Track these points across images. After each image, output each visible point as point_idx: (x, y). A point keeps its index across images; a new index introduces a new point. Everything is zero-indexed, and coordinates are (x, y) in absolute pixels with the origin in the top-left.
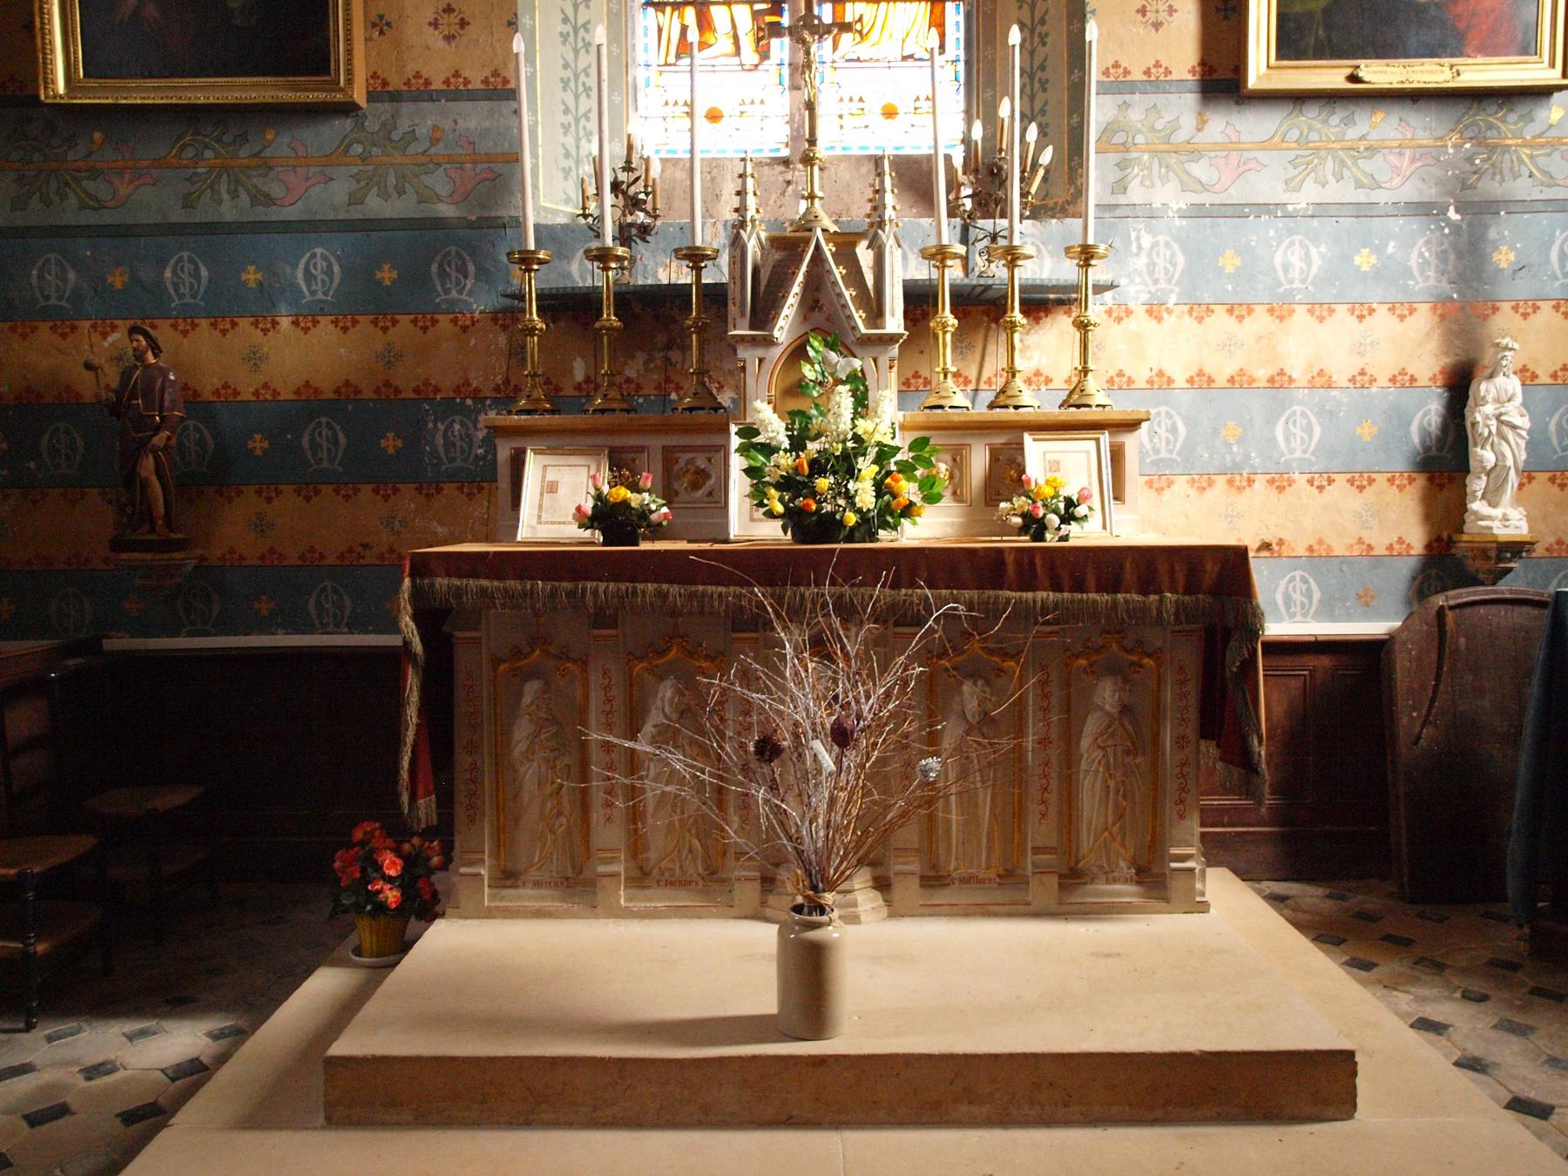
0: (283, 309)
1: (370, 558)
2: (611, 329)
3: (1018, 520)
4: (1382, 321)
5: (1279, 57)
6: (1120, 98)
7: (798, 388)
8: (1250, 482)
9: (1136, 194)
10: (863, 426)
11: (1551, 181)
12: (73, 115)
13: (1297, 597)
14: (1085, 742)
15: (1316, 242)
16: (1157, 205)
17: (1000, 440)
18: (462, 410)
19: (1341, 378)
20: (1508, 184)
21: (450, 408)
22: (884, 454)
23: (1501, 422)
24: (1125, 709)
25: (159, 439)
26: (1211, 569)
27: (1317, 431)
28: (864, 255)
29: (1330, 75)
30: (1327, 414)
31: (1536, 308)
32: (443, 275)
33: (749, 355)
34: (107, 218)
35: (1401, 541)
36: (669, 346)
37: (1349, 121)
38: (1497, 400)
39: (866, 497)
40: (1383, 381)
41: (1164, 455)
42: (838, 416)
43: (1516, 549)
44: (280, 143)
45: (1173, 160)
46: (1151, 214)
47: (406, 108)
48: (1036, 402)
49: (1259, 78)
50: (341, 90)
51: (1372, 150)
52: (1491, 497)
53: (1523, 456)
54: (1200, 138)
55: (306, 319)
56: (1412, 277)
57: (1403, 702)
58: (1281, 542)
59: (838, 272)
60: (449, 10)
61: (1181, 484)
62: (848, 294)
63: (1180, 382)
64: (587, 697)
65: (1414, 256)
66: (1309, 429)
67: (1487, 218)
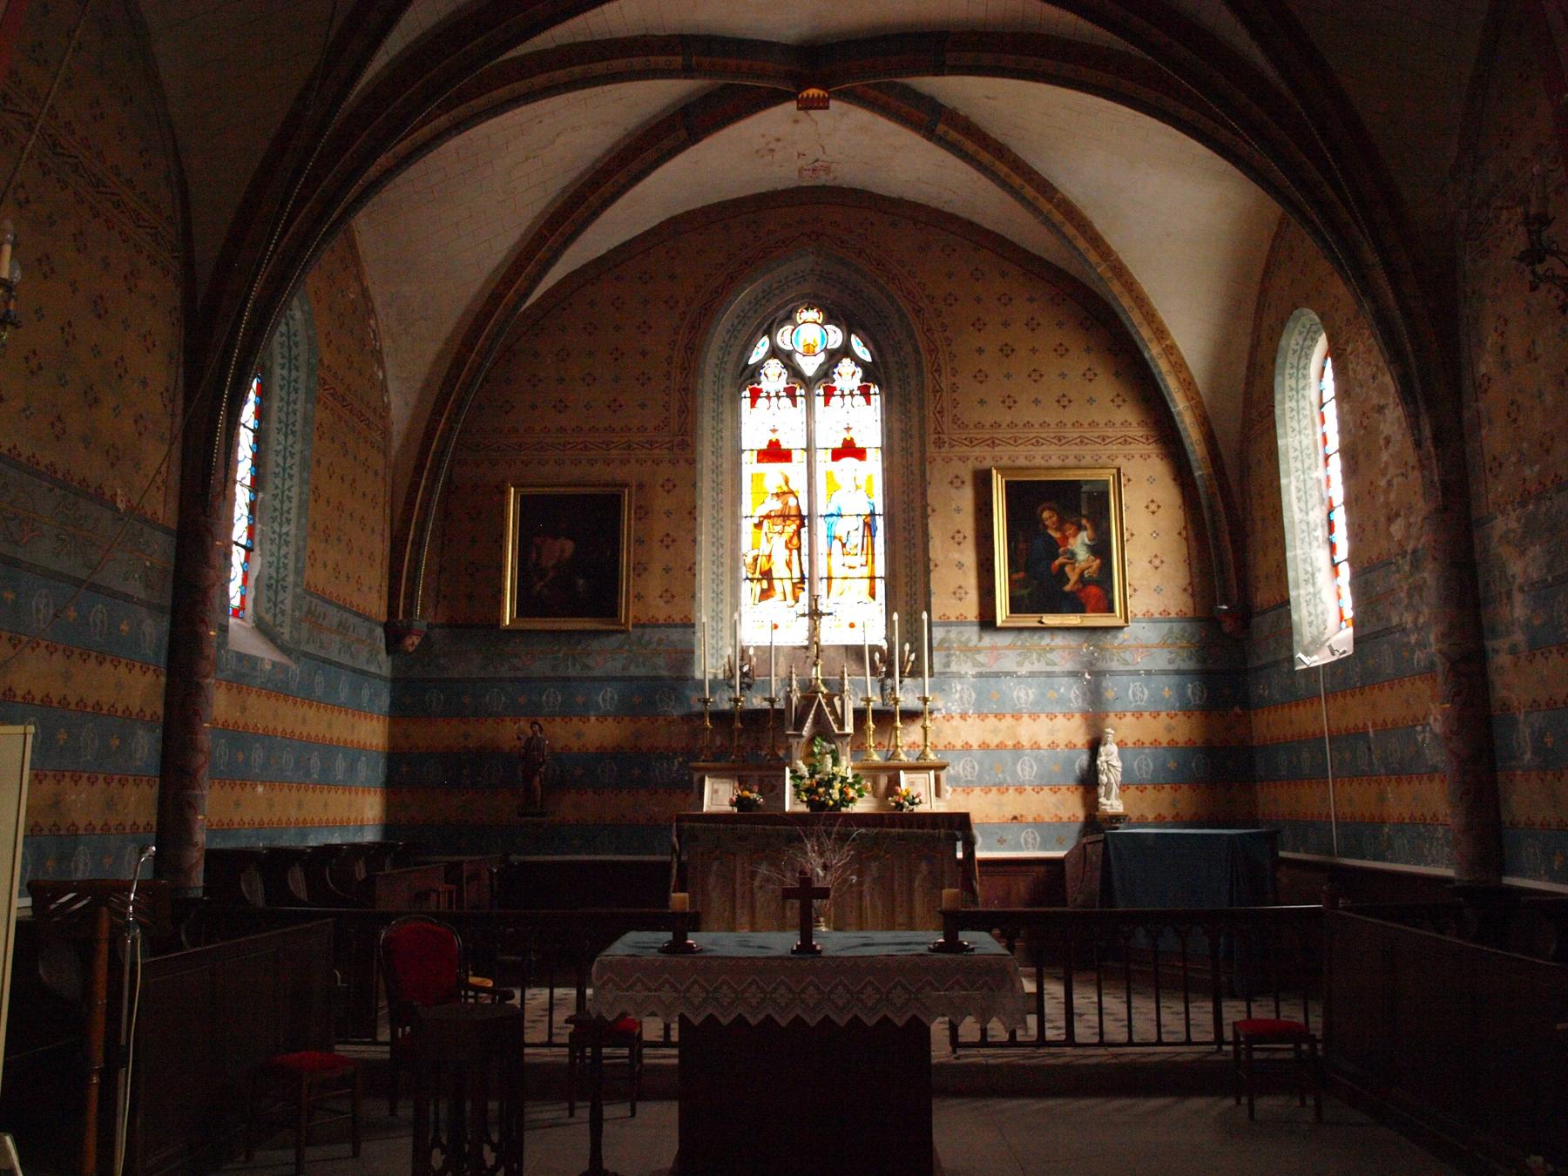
0: (592, 713)
2: (739, 729)
3: (893, 804)
4: (1060, 720)
5: (1011, 612)
6: (946, 628)
7: (812, 754)
8: (1007, 790)
9: (954, 668)
12: (508, 631)
13: (1030, 840)
15: (1031, 687)
16: (963, 672)
17: (892, 773)
19: (1044, 744)
20: (1109, 663)
23: (1108, 765)
24: (930, 873)
25: (542, 770)
27: (1035, 769)
28: (837, 701)
29: (1030, 620)
30: (1039, 760)
31: (1125, 715)
33: (794, 742)
35: (1074, 815)
37: (1042, 638)
38: (1107, 755)
39: (836, 795)
40: (1062, 746)
41: (969, 778)
42: (826, 766)
43: (1117, 818)
44: (595, 645)
45: (969, 654)
46: (960, 676)
47: (648, 630)
49: (1003, 622)
50: (622, 625)
51: (1052, 650)
52: (1107, 796)
53: (1119, 778)
55: (602, 717)
56: (1071, 702)
58: (1022, 816)
59: (827, 710)
61: (977, 791)
62: (831, 718)
63: (975, 746)
64: (735, 866)
65: (1072, 693)
66: (1031, 767)
67: (1102, 678)
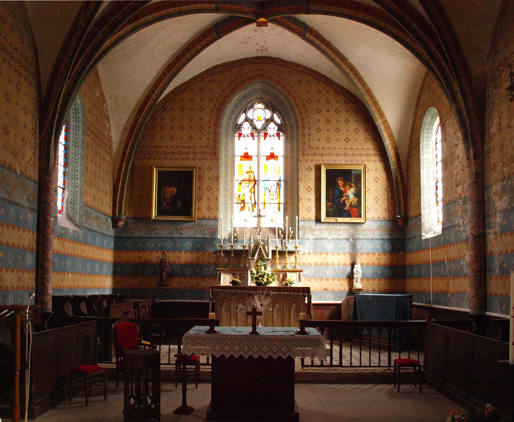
1: (194, 288)
5: (327, 216)
7: (257, 266)
9: (306, 236)
10: (265, 271)
11: (365, 236)
12: (155, 221)
13: (330, 297)
14: (292, 311)
17: (284, 273)
18: (209, 266)
19: (336, 264)
21: (207, 266)
22: (268, 275)
25: (166, 270)
26: (306, 290)
29: (333, 220)
30: (334, 270)
32: (206, 246)
33: (251, 261)
34: (158, 236)
36: (239, 257)
37: (336, 226)
39: (265, 280)
40: (342, 264)
44: (184, 226)
45: (311, 231)
46: (308, 239)
47: (202, 221)
48: (289, 268)
51: (340, 230)
53: (361, 276)
54: (316, 228)
57: (343, 312)
59: (263, 250)
60: (209, 207)
61: (313, 280)
62: (264, 253)
63: (313, 264)
66: (331, 272)
